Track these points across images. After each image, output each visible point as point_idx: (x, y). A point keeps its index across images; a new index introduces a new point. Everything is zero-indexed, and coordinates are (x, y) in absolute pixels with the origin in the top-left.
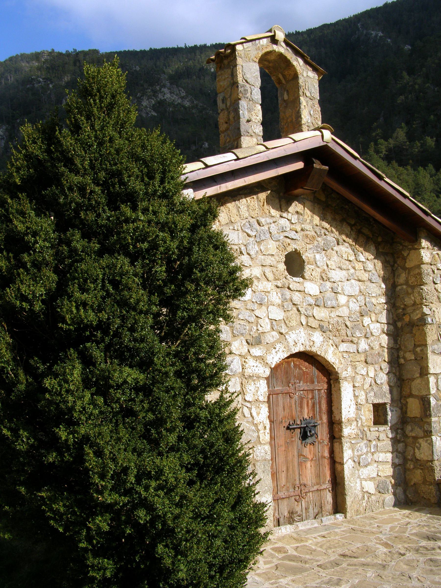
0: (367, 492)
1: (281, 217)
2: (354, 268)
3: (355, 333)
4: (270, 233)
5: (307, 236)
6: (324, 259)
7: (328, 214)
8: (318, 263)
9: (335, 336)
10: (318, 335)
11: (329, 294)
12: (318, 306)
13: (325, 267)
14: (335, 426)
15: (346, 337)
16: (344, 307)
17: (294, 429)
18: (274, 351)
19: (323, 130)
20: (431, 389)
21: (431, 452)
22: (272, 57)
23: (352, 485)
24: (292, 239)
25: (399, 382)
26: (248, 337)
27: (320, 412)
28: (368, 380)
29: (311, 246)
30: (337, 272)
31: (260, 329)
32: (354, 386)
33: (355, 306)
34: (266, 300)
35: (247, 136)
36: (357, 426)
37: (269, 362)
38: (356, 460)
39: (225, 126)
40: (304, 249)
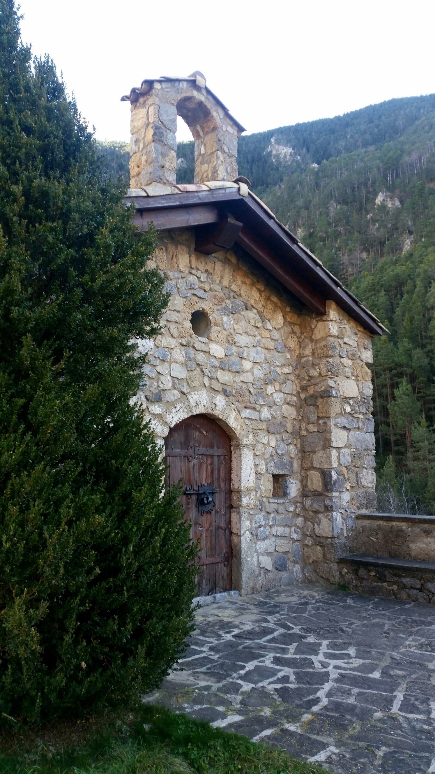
0: (264, 568)
1: (191, 273)
2: (260, 335)
3: (258, 401)
4: (178, 288)
5: (215, 297)
6: (232, 322)
7: (238, 277)
8: (225, 325)
9: (238, 402)
10: (221, 399)
11: (234, 359)
12: (223, 369)
13: (232, 331)
14: (233, 494)
15: (248, 404)
16: (249, 373)
17: (191, 494)
18: (174, 410)
19: (240, 183)
20: (333, 463)
21: (331, 529)
22: (192, 105)
23: (249, 559)
24: (200, 298)
25: (300, 455)
26: (148, 393)
27: (219, 478)
28: (270, 450)
29: (219, 307)
30: (244, 338)
31: (161, 386)
32: (255, 455)
33: (259, 373)
34: (169, 357)
35: (160, 182)
36: (256, 496)
37: (168, 421)
38: (254, 533)
39: (136, 170)
40: (212, 310)
